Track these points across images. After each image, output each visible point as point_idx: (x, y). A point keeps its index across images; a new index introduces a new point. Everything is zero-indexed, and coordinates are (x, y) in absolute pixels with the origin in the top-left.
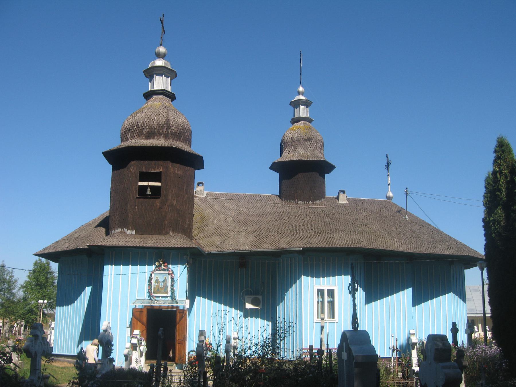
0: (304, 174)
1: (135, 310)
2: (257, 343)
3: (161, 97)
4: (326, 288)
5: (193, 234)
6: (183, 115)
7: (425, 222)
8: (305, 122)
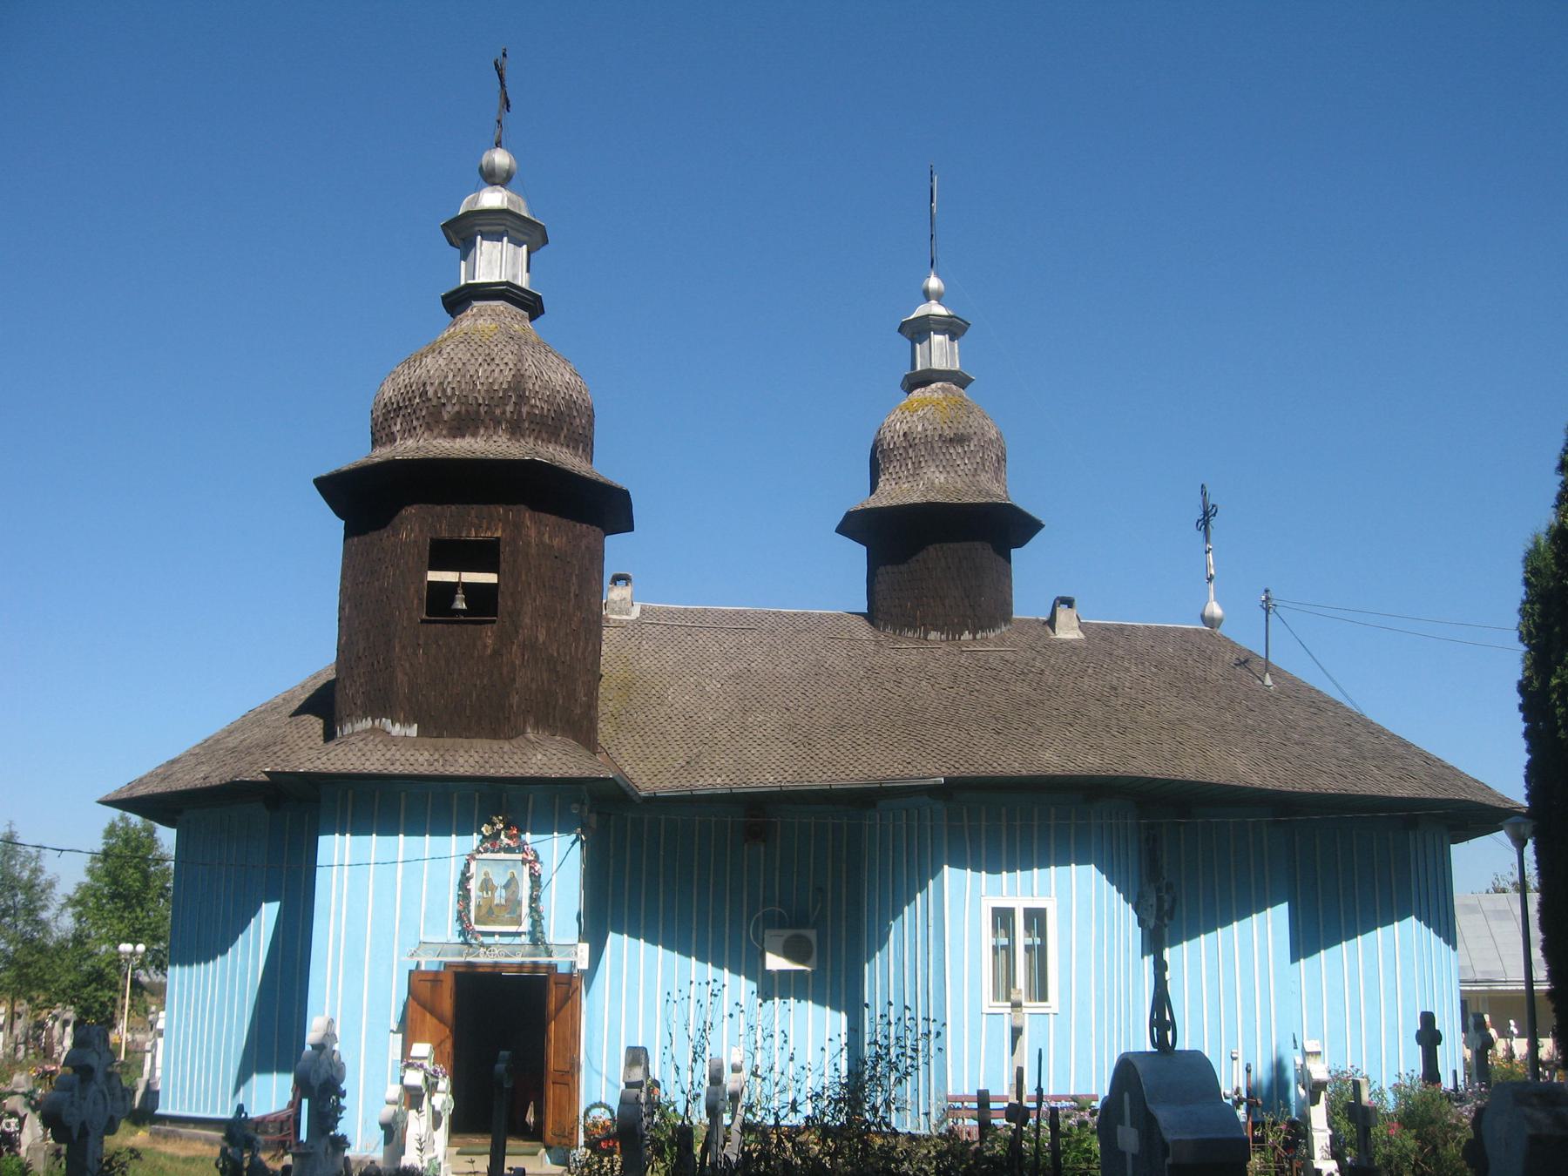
0: (945, 546)
1: (415, 977)
2: (819, 1089)
3: (500, 305)
4: (1019, 904)
5: (600, 738)
6: (566, 361)
7: (1323, 696)
8: (946, 385)
